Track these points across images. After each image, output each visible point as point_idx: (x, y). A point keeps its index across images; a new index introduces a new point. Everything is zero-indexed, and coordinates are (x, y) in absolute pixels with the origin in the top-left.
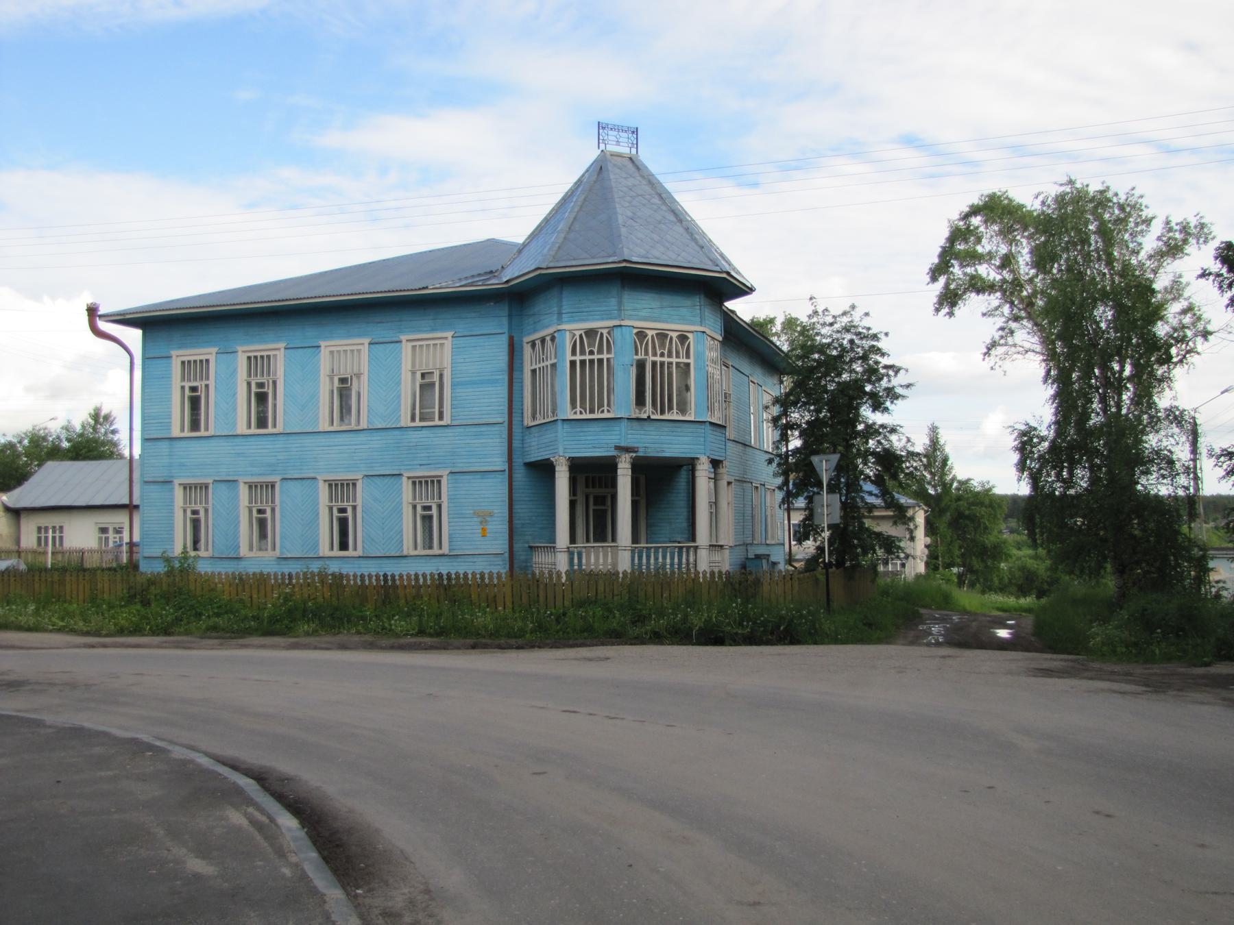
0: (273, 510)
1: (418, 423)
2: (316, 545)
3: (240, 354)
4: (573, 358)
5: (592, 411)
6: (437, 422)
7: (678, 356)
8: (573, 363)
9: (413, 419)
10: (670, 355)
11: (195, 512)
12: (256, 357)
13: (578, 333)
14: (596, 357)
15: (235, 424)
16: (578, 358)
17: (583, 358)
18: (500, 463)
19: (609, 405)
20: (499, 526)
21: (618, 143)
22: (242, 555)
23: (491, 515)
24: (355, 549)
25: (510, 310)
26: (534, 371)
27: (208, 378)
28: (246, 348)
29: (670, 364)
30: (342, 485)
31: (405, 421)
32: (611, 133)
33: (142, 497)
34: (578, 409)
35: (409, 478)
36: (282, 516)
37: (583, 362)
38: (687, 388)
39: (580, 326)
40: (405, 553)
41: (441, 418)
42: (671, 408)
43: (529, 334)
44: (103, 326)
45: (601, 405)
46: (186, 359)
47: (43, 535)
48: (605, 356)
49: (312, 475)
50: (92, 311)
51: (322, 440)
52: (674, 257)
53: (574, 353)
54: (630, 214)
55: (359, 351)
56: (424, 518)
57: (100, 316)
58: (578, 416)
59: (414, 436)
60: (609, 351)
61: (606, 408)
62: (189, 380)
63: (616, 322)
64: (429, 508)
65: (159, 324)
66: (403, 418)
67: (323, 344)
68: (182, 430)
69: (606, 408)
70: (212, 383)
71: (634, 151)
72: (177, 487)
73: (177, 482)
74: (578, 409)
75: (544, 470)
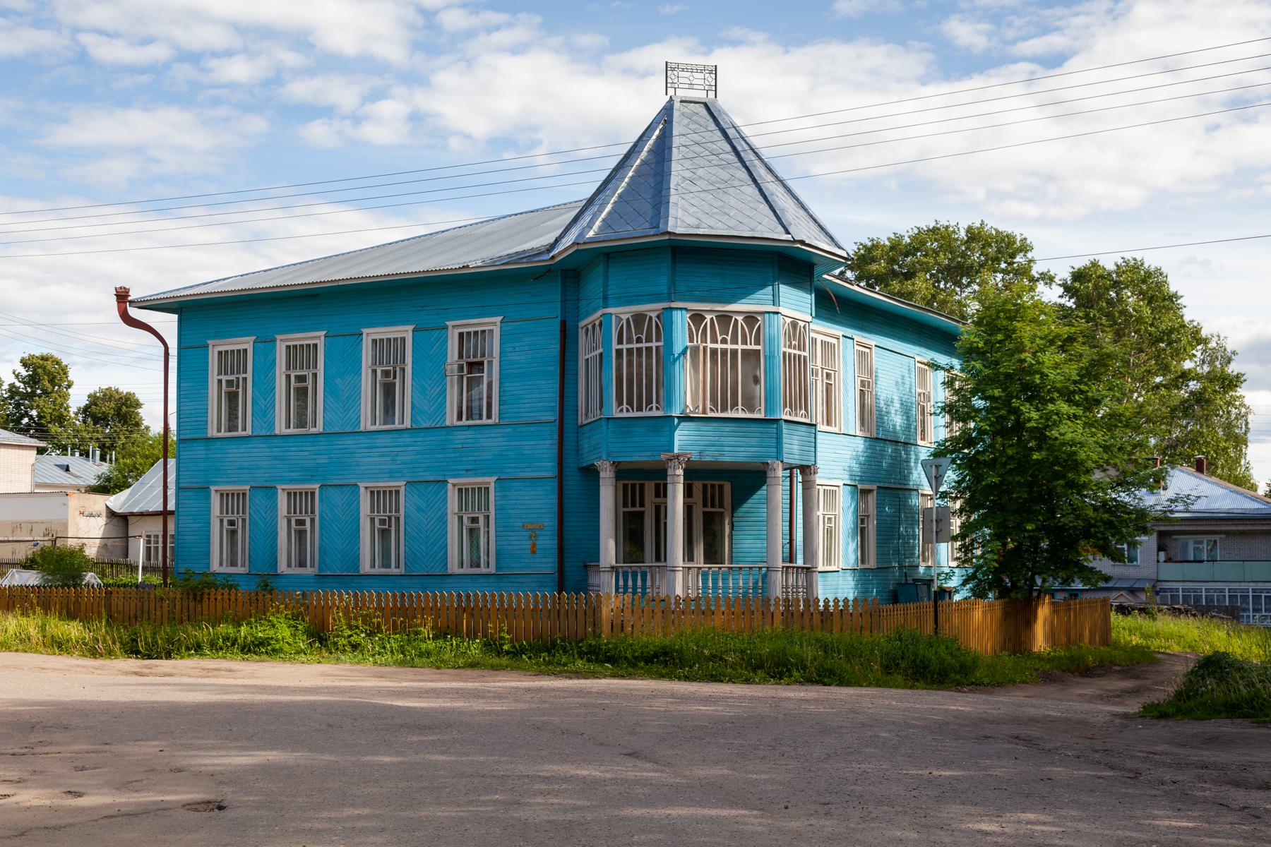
0: (313, 520)
1: (464, 422)
2: (356, 562)
3: (450, 328)
4: (620, 347)
5: (640, 409)
6: (485, 421)
7: (744, 342)
8: (619, 352)
9: (460, 418)
10: (735, 341)
11: (232, 523)
12: (295, 346)
13: (624, 317)
14: (644, 345)
15: (272, 424)
16: (625, 346)
17: (630, 346)
18: (548, 468)
19: (657, 402)
20: (548, 542)
21: (691, 86)
22: (279, 571)
23: (541, 528)
24: (398, 566)
25: (564, 293)
26: (587, 360)
27: (245, 372)
28: (283, 337)
29: (734, 352)
30: (385, 492)
31: (451, 419)
32: (681, 74)
33: (177, 504)
34: (625, 406)
35: (454, 485)
36: (321, 528)
37: (630, 351)
38: (756, 380)
39: (624, 312)
40: (450, 572)
41: (489, 416)
42: (735, 404)
43: (586, 317)
44: (134, 312)
45: (649, 401)
46: (377, 337)
47: (152, 545)
48: (654, 344)
49: (353, 481)
50: (122, 296)
51: (364, 440)
52: (732, 223)
53: (620, 341)
54: (688, 174)
55: (491, 331)
56: (471, 531)
57: (131, 302)
58: (625, 415)
59: (460, 436)
60: (658, 340)
61: (654, 405)
62: (226, 374)
63: (665, 305)
64: (474, 520)
65: (201, 313)
66: (448, 417)
67: (365, 331)
68: (219, 430)
69: (654, 405)
70: (249, 375)
71: (712, 94)
72: (213, 493)
73: (213, 488)
74: (625, 406)
75: (591, 473)
